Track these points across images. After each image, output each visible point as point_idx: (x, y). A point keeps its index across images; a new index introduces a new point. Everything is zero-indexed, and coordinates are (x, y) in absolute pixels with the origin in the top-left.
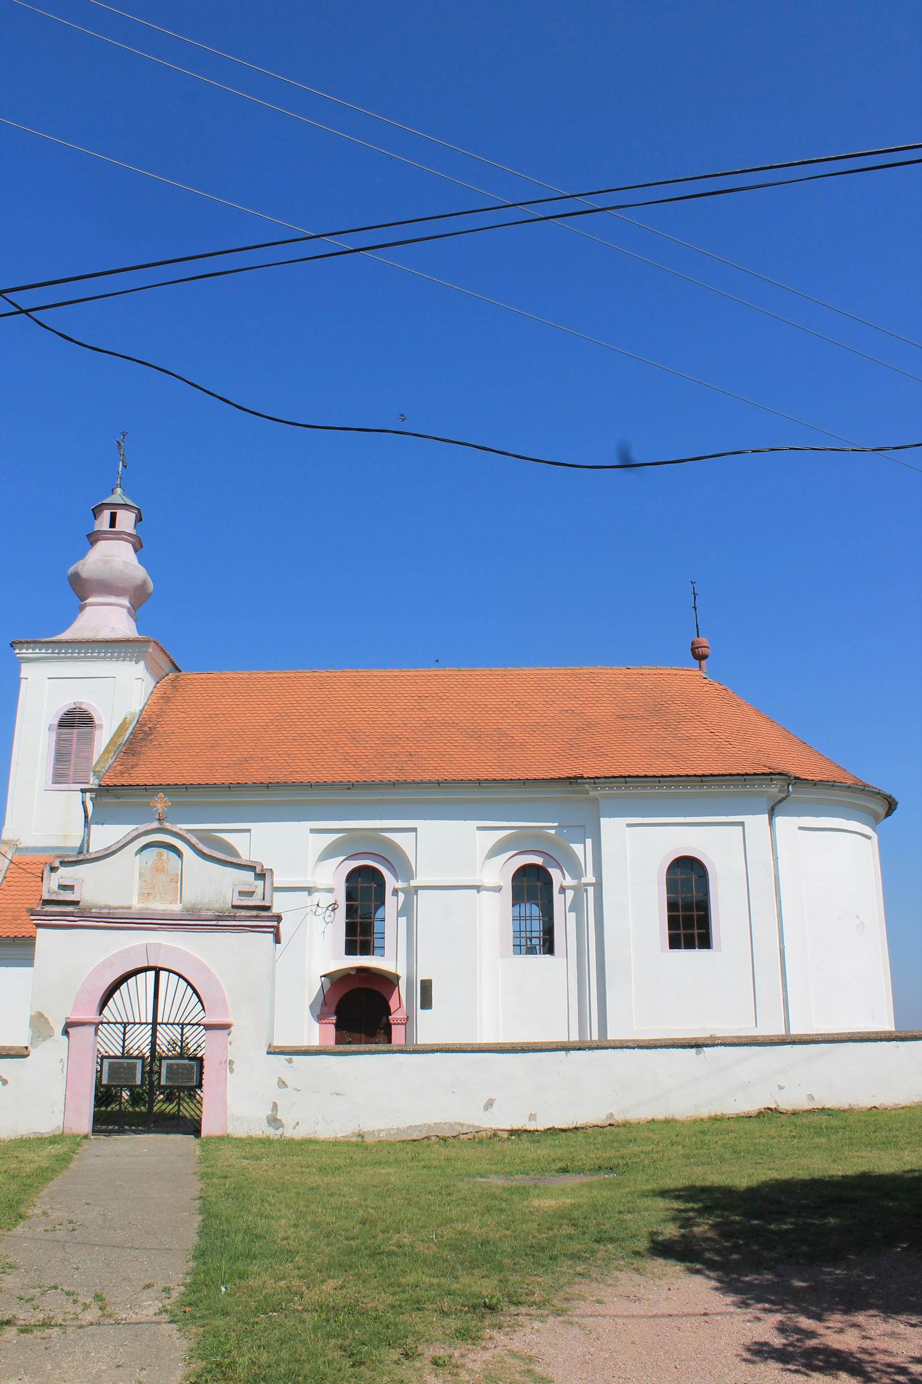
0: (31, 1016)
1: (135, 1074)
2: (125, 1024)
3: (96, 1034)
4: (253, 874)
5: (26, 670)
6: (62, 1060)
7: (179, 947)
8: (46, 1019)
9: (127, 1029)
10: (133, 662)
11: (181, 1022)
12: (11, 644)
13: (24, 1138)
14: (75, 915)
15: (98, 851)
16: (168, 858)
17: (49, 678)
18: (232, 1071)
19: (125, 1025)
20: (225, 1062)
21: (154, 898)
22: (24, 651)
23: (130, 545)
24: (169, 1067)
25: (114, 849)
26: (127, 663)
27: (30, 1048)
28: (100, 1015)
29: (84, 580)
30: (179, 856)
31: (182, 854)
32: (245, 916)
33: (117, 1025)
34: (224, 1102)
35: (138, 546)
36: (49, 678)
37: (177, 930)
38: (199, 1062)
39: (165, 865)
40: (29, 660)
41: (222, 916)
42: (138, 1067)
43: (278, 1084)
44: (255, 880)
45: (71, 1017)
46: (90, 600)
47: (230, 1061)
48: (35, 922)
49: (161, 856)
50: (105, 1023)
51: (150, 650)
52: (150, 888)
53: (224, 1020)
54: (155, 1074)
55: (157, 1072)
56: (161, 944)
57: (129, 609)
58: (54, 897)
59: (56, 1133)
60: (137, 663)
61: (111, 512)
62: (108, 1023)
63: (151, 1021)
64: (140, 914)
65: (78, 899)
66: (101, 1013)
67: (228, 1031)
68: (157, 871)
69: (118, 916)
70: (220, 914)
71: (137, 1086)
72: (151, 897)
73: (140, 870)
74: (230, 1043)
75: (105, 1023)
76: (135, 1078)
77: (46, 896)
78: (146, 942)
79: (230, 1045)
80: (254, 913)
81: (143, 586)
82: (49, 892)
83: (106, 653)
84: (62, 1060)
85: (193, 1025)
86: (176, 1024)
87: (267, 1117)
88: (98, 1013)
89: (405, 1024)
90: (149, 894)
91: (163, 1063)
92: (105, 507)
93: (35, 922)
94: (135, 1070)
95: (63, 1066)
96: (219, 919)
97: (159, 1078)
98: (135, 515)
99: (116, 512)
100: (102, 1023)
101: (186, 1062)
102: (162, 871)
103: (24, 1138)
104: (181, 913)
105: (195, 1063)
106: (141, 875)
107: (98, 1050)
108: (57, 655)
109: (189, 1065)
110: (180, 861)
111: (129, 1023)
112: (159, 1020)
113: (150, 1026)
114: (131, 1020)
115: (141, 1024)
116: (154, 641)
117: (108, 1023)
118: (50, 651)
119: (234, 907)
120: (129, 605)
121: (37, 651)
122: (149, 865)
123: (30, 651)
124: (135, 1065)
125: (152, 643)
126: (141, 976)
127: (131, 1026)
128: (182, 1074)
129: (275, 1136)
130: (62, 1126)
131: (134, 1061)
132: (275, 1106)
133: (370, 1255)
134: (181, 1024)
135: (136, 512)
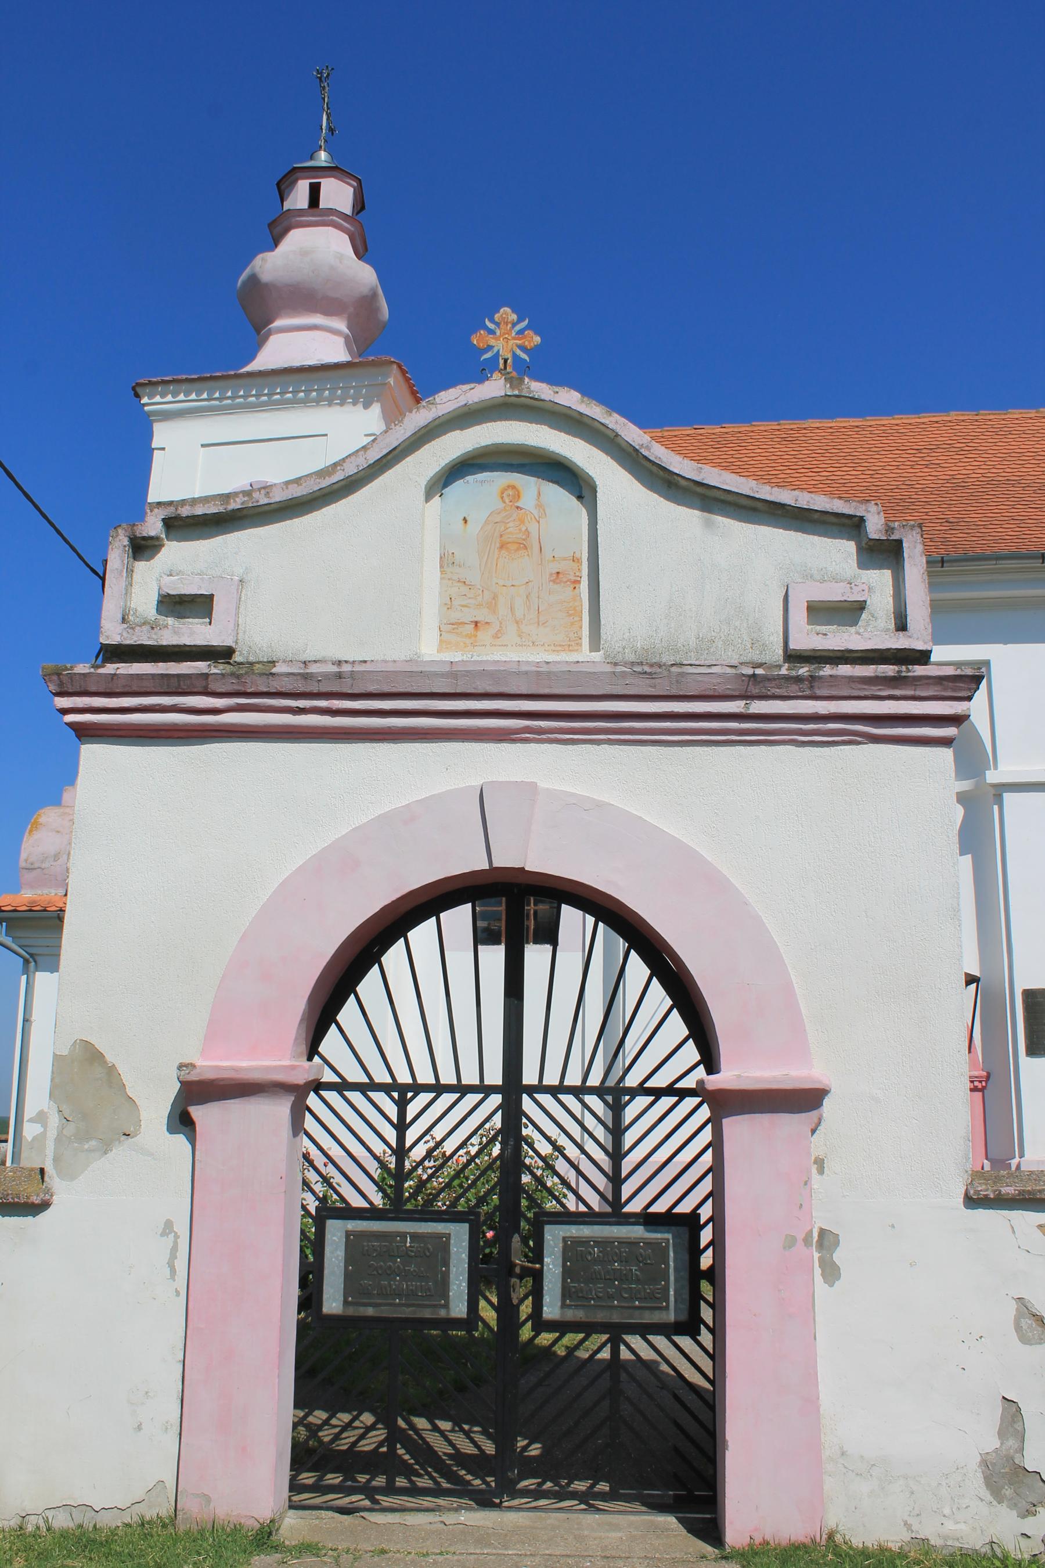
0: (56, 1057)
1: (446, 1276)
2: (403, 1089)
3: (297, 1127)
4: (850, 547)
5: (162, 434)
6: (168, 1227)
7: (605, 797)
8: (111, 1071)
9: (412, 1110)
10: (360, 406)
11: (611, 1082)
12: (134, 388)
13: (30, 1528)
14: (214, 686)
15: (297, 481)
16: (539, 506)
17: (202, 446)
18: (831, 1272)
19: (403, 1095)
20: (807, 1240)
21: (496, 636)
22: (158, 399)
23: (347, 237)
24: (572, 1249)
25: (350, 469)
26: (348, 408)
27: (54, 1179)
28: (310, 1058)
29: (266, 285)
30: (580, 497)
31: (593, 489)
32: (851, 679)
33: (538, 1096)
34: (811, 1403)
35: (361, 250)
36: (202, 446)
37: (588, 738)
38: (684, 1232)
39: (533, 528)
40: (167, 416)
41: (766, 679)
42: (453, 1249)
43: (1018, 1328)
44: (862, 565)
45: (200, 1062)
46: (278, 323)
47: (822, 1232)
48: (70, 718)
49: (518, 496)
50: (330, 1086)
51: (391, 381)
52: (480, 605)
53: (794, 1073)
54: (521, 1278)
55: (526, 1272)
56: (533, 786)
57: (346, 338)
58: (143, 638)
59: (150, 1514)
60: (366, 406)
61: (310, 183)
62: (342, 1087)
63: (499, 1082)
64: (454, 675)
65: (229, 642)
66: (313, 1051)
67: (814, 1114)
68: (502, 547)
69: (372, 688)
70: (759, 671)
71: (456, 1323)
72: (484, 635)
73: (443, 546)
74: (820, 1163)
75: (330, 1086)
76: (445, 1295)
77: (112, 633)
78: (477, 782)
79: (821, 1171)
80: (889, 670)
81: (367, 302)
82: (124, 620)
83: (308, 392)
84: (168, 1227)
85: (658, 1093)
86: (592, 1090)
87: (985, 1463)
88: (303, 1049)
89: (982, 1090)
90: (476, 623)
91: (548, 1236)
92: (299, 174)
93: (70, 718)
94: (446, 1263)
95: (174, 1249)
96: (755, 691)
97: (537, 1293)
98: (352, 190)
99: (320, 183)
100: (318, 1086)
101: (638, 1232)
102: (523, 546)
103: (30, 1528)
104: (609, 668)
105: (669, 1236)
106: (446, 561)
107: (306, 1157)
108: (217, 403)
109: (648, 1244)
110: (584, 513)
111: (418, 1088)
112: (529, 1077)
113: (496, 1099)
114: (425, 1077)
115: (463, 1090)
116: (400, 366)
117: (342, 1087)
118: (205, 396)
119: (793, 657)
120: (346, 331)
121: (181, 397)
122: (474, 528)
123: (169, 398)
124: (443, 1243)
125: (395, 366)
126: (422, 935)
127: (424, 1098)
128: (624, 1278)
129: (1024, 1542)
130: (171, 1484)
131: (440, 1228)
132: (1012, 1411)
133: (400, 1175)
134: (610, 1091)
135: (355, 184)
